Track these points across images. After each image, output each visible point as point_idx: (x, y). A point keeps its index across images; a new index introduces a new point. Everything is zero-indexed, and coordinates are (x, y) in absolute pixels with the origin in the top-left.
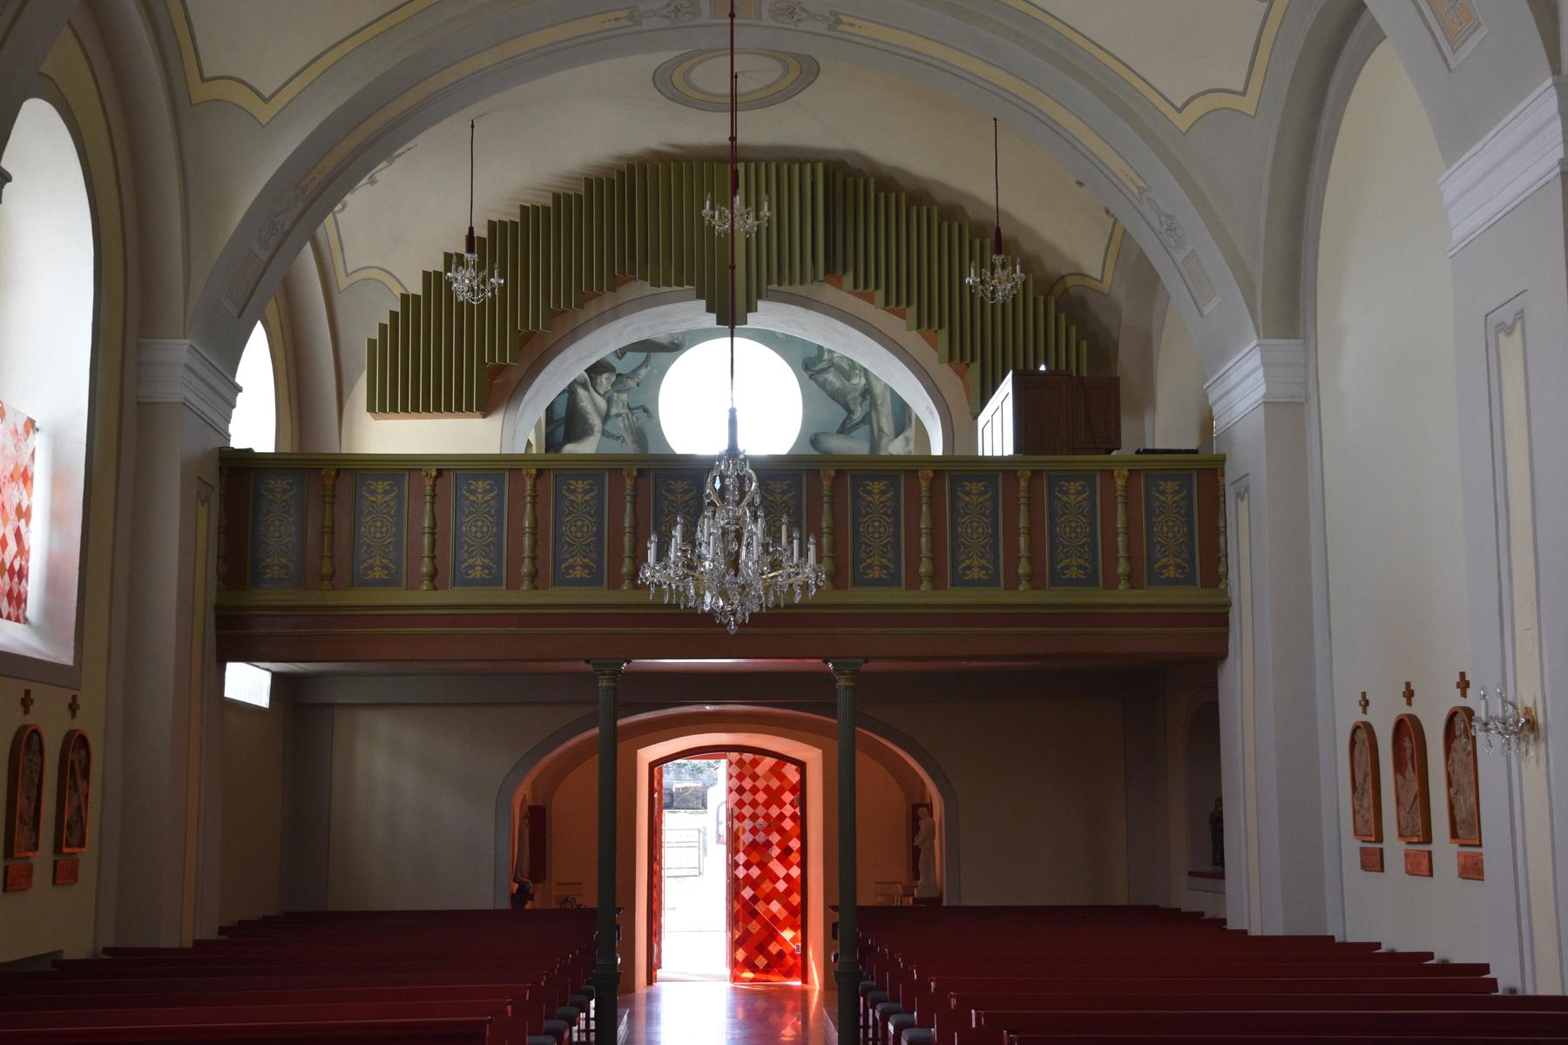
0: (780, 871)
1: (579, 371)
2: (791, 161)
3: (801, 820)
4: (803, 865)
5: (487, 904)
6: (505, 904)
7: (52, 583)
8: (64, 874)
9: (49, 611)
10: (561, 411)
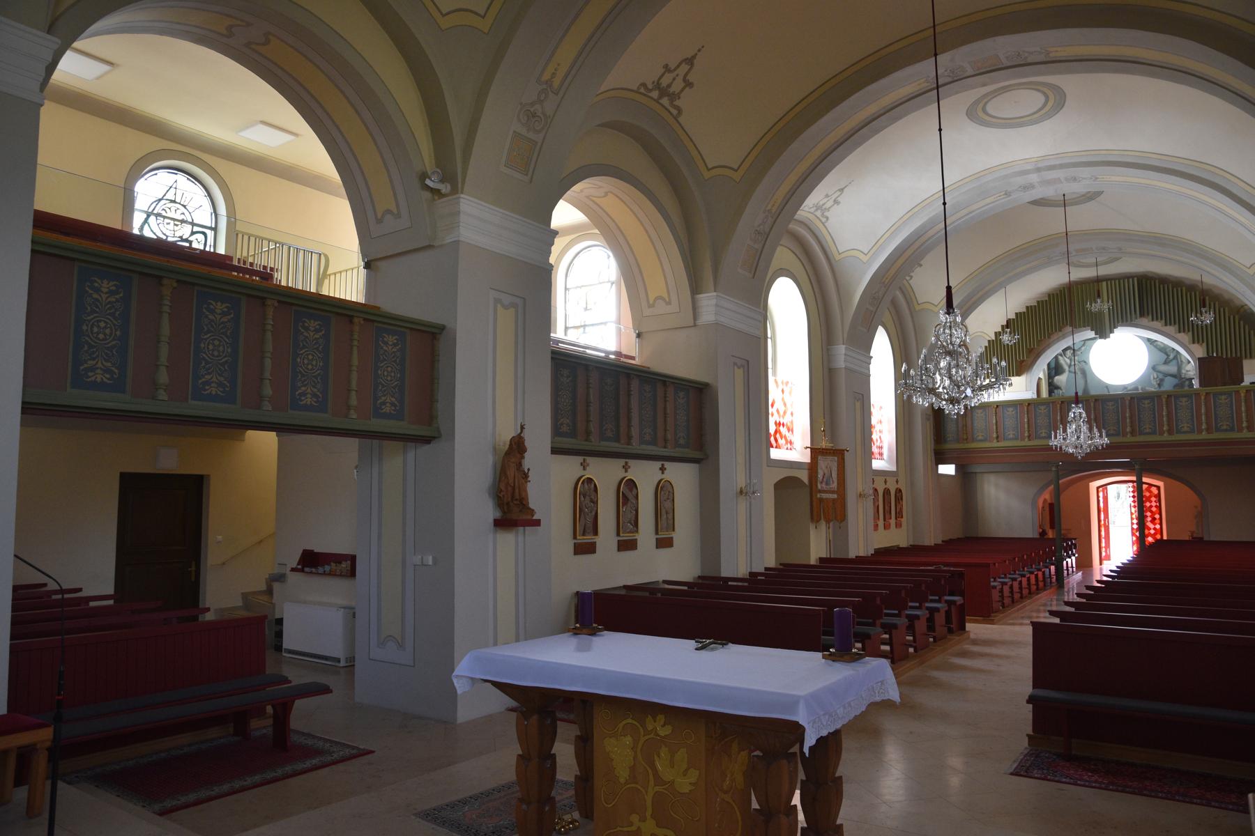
0: (1151, 526)
1: (1060, 351)
2: (1128, 278)
3: (1159, 508)
4: (1161, 524)
5: (1030, 535)
6: (1037, 536)
7: (890, 449)
8: (898, 525)
9: (889, 457)
10: (1053, 365)
